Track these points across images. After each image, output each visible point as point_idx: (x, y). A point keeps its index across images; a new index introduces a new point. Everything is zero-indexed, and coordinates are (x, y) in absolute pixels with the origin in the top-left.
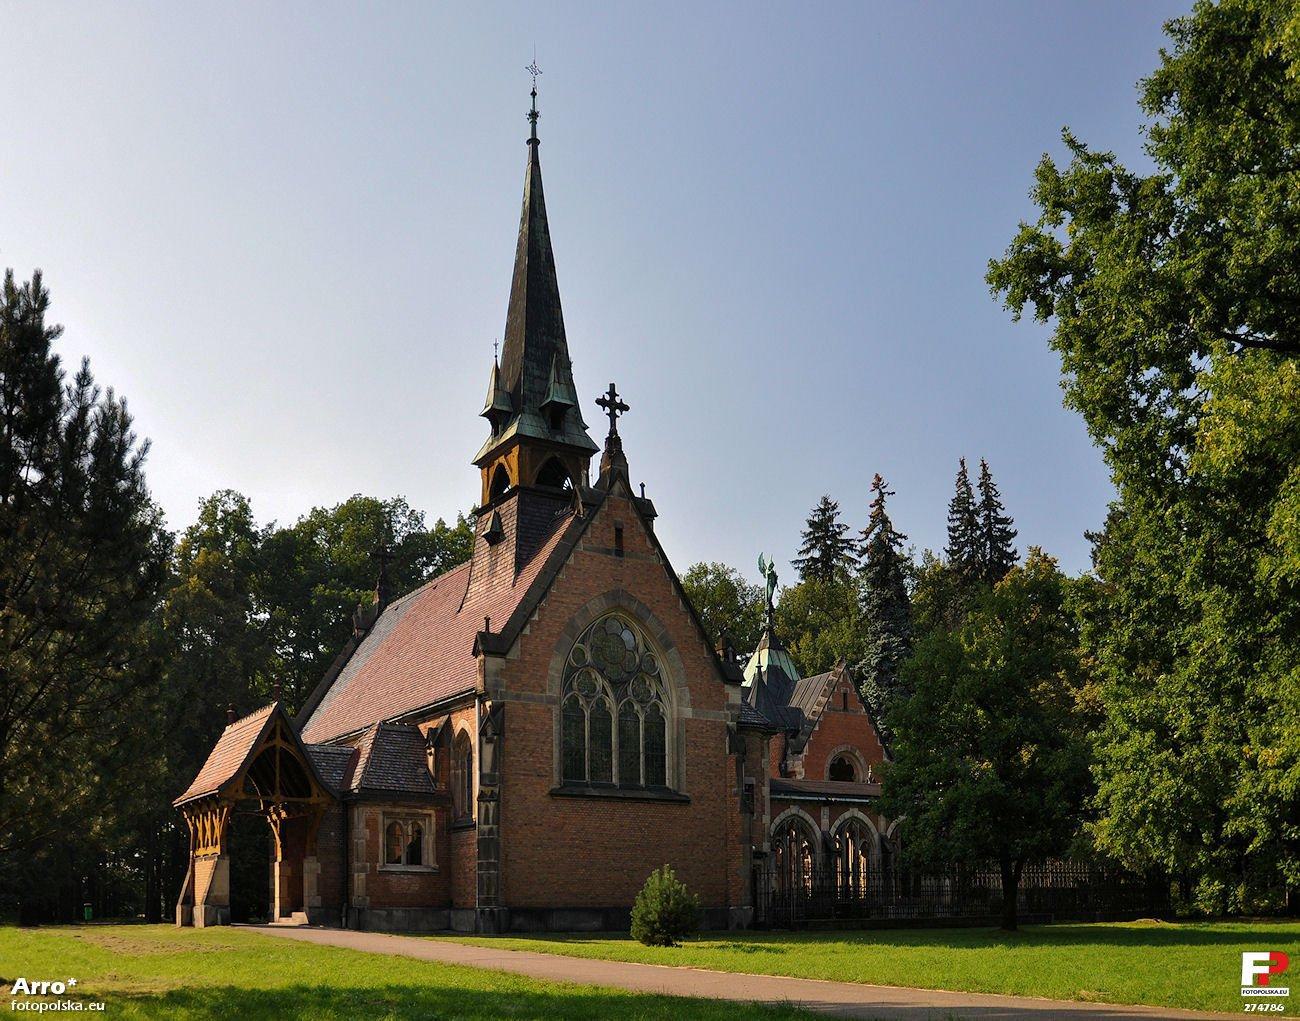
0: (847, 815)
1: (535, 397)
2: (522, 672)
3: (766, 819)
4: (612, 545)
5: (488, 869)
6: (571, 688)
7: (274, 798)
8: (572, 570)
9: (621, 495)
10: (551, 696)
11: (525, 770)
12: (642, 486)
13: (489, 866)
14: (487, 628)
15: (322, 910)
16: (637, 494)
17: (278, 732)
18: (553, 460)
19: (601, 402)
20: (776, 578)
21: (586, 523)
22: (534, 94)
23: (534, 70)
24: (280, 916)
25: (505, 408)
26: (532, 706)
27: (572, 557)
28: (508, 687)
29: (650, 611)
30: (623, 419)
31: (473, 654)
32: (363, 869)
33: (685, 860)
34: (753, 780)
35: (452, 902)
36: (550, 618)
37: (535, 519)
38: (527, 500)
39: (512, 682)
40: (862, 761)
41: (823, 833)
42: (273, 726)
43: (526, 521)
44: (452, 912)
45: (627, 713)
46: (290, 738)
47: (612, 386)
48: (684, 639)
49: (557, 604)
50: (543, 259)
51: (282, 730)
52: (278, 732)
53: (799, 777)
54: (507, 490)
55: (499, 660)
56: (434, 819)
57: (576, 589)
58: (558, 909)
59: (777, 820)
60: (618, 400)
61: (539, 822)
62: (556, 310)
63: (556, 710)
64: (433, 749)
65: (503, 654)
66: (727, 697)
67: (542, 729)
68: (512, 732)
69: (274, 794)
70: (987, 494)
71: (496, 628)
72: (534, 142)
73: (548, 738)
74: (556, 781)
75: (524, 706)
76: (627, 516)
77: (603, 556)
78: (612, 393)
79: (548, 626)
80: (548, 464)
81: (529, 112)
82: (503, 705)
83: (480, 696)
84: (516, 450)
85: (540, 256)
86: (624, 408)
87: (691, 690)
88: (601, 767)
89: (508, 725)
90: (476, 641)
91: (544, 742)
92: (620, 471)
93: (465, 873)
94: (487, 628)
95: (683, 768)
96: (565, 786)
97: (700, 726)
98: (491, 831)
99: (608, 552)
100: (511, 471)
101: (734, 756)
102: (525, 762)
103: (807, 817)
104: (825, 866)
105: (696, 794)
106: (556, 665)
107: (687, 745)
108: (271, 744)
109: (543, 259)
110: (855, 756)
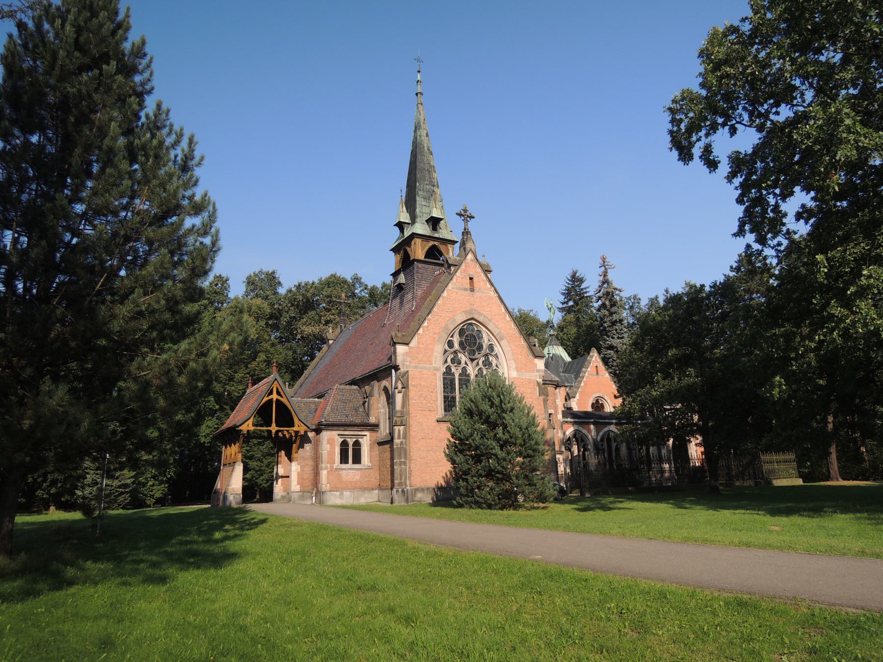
4: (468, 286)
6: (446, 361)
15: (300, 493)
18: (434, 246)
27: (445, 292)
29: (490, 321)
39: (413, 359)
50: (426, 149)
56: (368, 437)
59: (601, 434)
66: (536, 365)
77: (463, 292)
85: (424, 147)
86: (472, 217)
87: (516, 362)
98: (402, 443)
99: (465, 289)
101: (542, 398)
108: (270, 397)
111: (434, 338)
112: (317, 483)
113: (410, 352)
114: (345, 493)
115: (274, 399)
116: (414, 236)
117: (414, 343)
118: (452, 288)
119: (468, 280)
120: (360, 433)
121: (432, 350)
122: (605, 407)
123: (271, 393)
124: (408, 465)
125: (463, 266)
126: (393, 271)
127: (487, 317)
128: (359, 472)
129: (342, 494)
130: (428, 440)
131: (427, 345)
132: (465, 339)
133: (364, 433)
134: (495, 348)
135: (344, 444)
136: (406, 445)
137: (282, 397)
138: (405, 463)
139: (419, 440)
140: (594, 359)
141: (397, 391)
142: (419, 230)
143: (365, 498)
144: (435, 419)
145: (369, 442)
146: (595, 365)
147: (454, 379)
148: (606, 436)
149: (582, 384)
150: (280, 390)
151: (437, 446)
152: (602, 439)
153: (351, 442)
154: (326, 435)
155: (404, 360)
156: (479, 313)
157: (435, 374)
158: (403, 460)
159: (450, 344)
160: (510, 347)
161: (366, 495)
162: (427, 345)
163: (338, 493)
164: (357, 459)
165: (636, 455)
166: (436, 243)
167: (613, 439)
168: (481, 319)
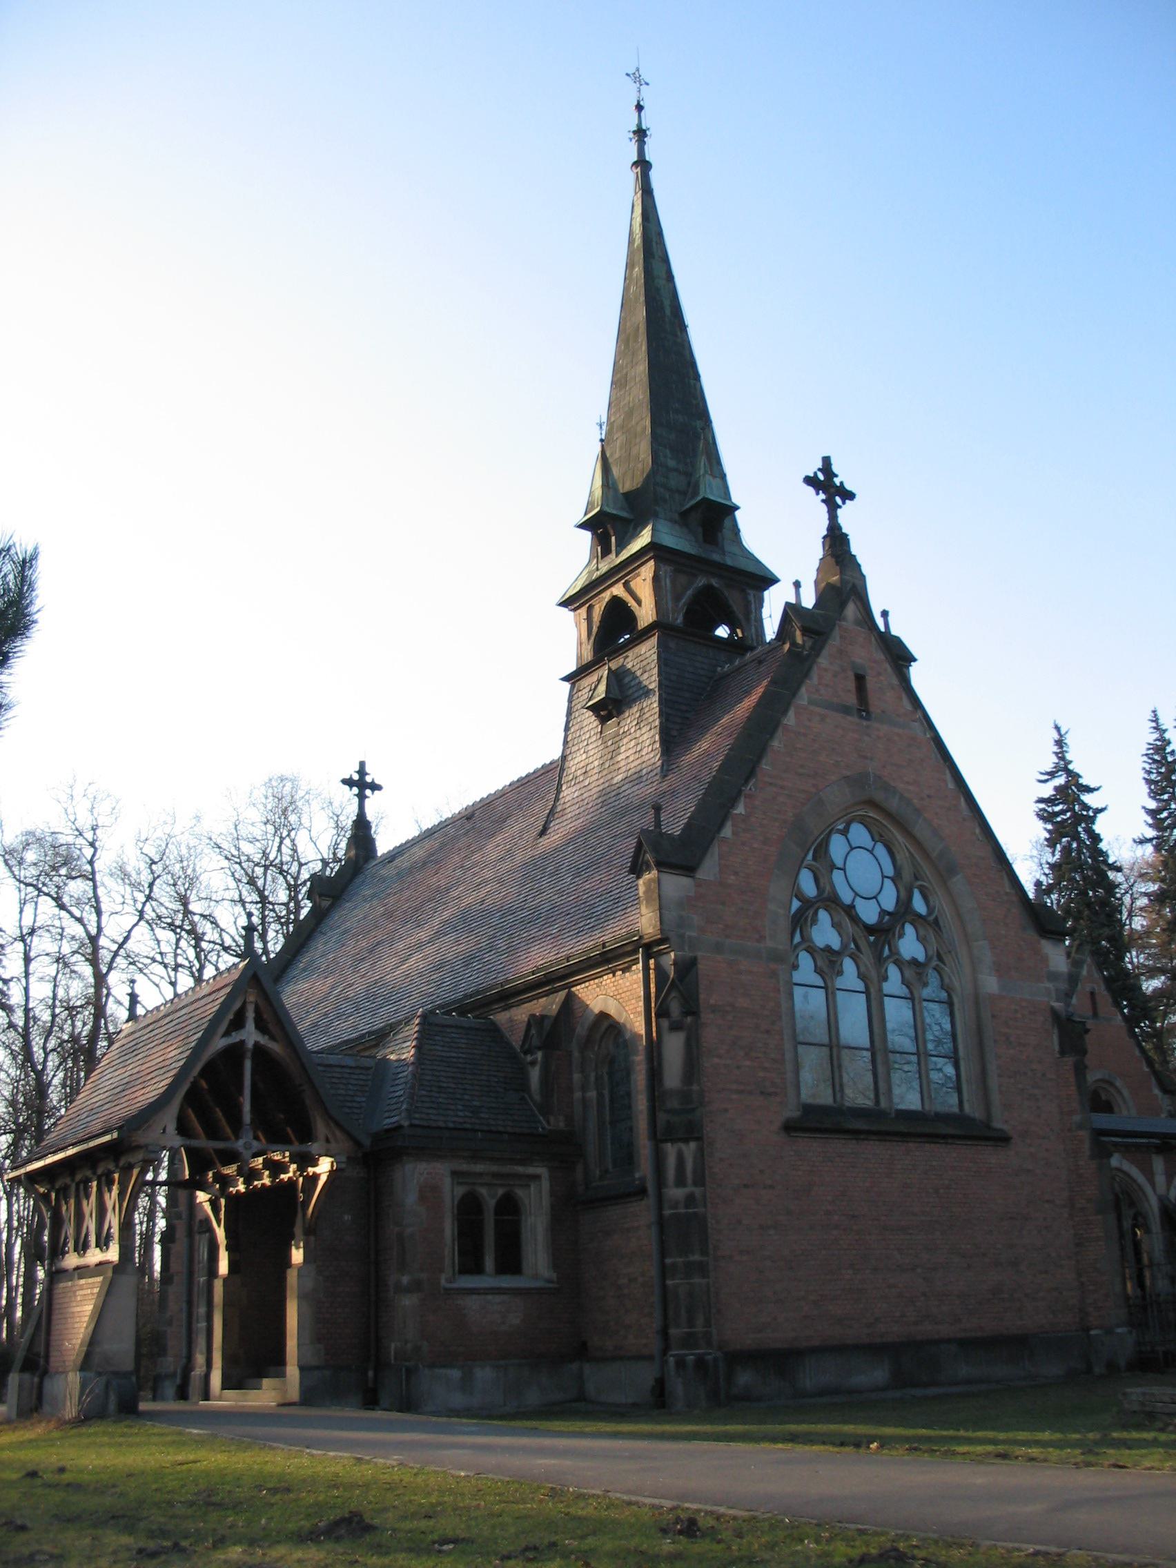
4: (852, 700)
7: (241, 1142)
14: (658, 823)
17: (250, 1015)
18: (709, 588)
23: (637, 77)
24: (224, 1387)
25: (624, 514)
27: (791, 713)
30: (848, 516)
32: (416, 1286)
35: (584, 1344)
38: (672, 645)
40: (1126, 1093)
42: (237, 1005)
47: (362, 764)
51: (257, 1011)
52: (250, 1015)
54: (622, 640)
55: (684, 881)
56: (546, 1184)
57: (802, 766)
58: (814, 1351)
62: (692, 382)
64: (539, 1055)
65: (688, 869)
66: (1045, 959)
68: (713, 1012)
69: (237, 1137)
71: (674, 825)
72: (643, 165)
78: (362, 771)
82: (693, 962)
83: (648, 948)
84: (647, 570)
86: (375, 787)
89: (708, 998)
90: (639, 846)
91: (768, 1032)
94: (658, 823)
95: (994, 1082)
98: (690, 1200)
99: (845, 710)
100: (639, 602)
101: (1070, 1060)
108: (235, 1038)
110: (1116, 1088)
115: (250, 1044)
117: (708, 869)
118: (811, 702)
119: (851, 685)
120: (520, 1169)
123: (238, 1023)
126: (572, 667)
133: (531, 1170)
135: (469, 1209)
137: (273, 1038)
138: (702, 1269)
140: (1084, 972)
145: (546, 1201)
146: (1088, 989)
153: (490, 1198)
158: (696, 1257)
163: (455, 1374)
164: (510, 1262)
166: (714, 582)
168: (893, 804)
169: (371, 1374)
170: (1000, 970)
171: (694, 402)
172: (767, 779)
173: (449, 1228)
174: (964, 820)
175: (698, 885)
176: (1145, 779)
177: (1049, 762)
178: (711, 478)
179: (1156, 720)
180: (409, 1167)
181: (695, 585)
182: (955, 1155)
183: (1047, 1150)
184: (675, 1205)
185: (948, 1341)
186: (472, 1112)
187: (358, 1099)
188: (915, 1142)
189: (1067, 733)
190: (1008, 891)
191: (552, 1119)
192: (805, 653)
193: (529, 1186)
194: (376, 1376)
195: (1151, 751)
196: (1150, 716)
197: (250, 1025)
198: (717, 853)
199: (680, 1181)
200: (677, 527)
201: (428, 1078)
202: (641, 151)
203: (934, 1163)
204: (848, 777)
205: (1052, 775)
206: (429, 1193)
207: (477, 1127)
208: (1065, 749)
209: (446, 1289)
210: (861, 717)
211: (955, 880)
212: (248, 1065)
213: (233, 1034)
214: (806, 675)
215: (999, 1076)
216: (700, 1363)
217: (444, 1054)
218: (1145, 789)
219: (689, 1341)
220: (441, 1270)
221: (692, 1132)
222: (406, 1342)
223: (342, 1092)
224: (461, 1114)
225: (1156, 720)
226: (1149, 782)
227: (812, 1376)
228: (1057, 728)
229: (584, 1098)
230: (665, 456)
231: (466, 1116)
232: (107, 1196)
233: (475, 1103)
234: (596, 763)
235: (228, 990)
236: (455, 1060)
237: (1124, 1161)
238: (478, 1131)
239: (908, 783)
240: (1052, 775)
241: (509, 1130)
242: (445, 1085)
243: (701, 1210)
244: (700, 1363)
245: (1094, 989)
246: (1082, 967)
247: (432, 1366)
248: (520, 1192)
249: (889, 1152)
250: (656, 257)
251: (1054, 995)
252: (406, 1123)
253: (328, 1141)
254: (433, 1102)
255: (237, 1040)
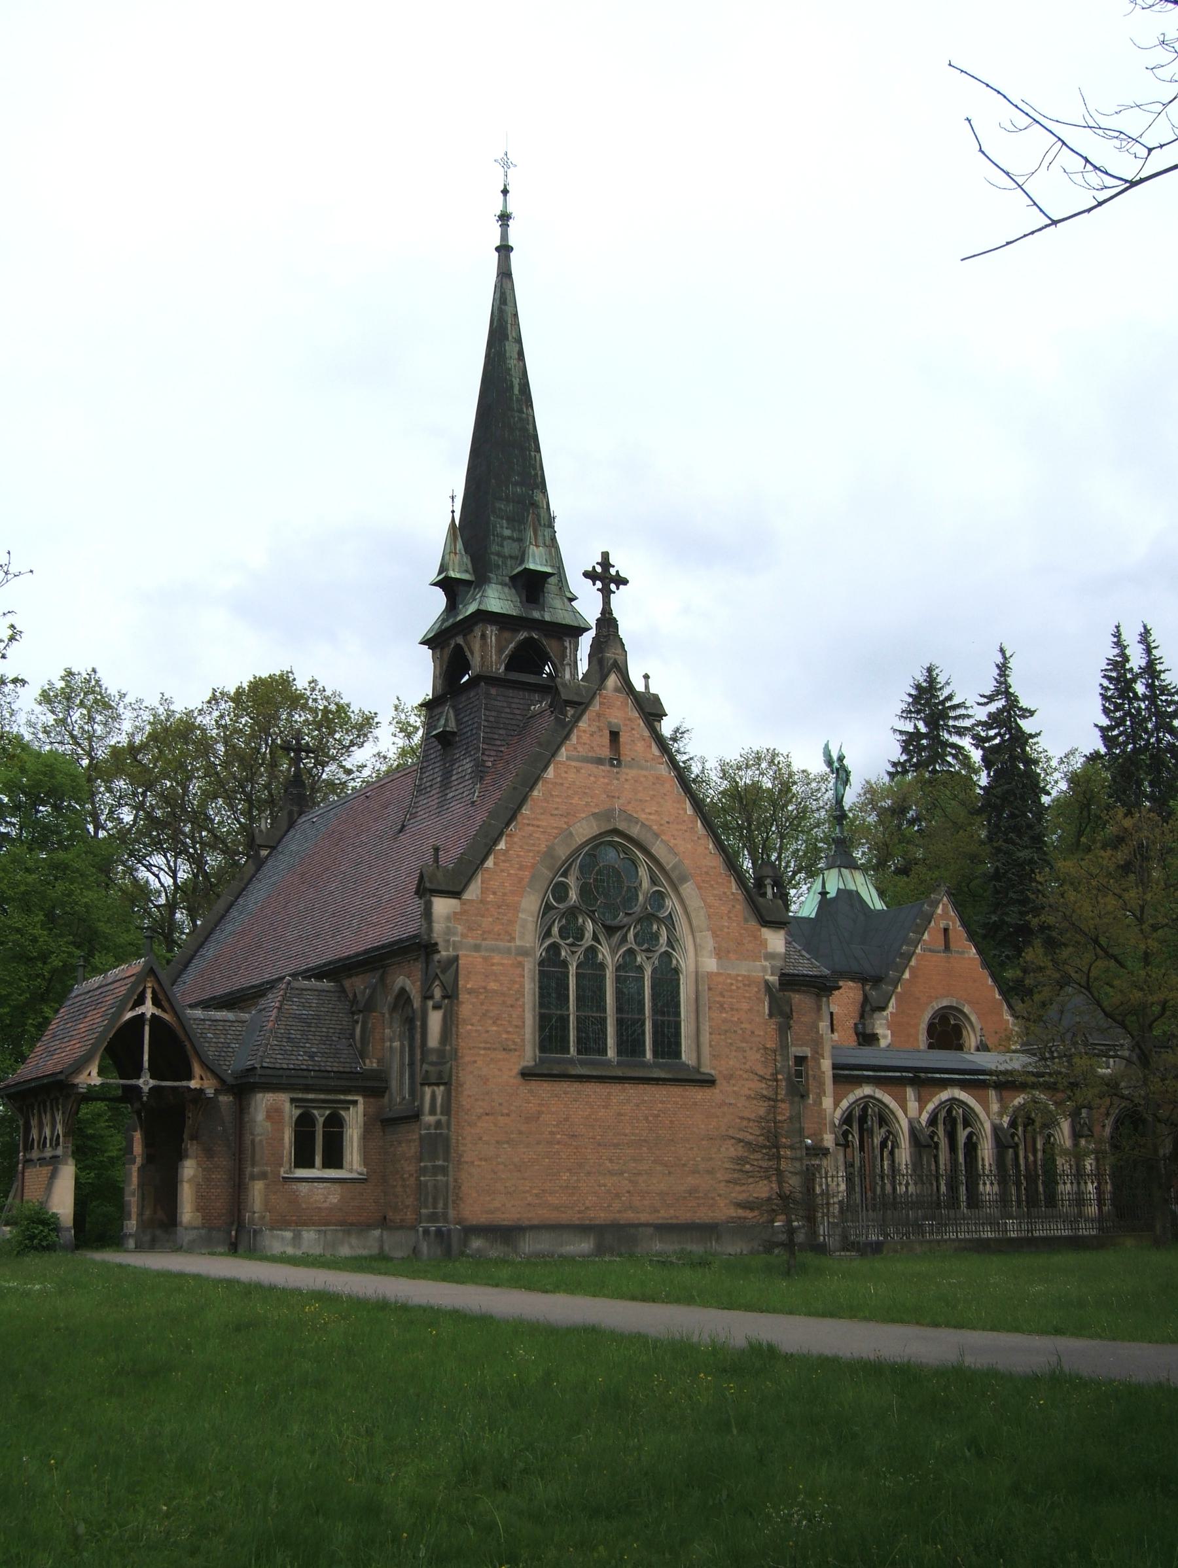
0: (945, 1095)
1: (505, 563)
2: (483, 916)
3: (827, 1102)
4: (606, 752)
5: (435, 1174)
6: (548, 934)
8: (551, 786)
9: (617, 690)
10: (522, 946)
11: (486, 1042)
12: (646, 677)
13: (437, 1170)
16: (639, 686)
17: (149, 995)
18: (529, 641)
19: (590, 575)
20: (848, 773)
21: (570, 726)
22: (505, 192)
26: (497, 959)
27: (551, 769)
28: (463, 936)
29: (657, 836)
31: (417, 893)
33: (711, 1159)
34: (807, 1051)
36: (521, 847)
37: (503, 715)
39: (470, 929)
41: (910, 1122)
43: (492, 719)
44: (385, 1232)
45: (627, 965)
46: (165, 1004)
47: (605, 556)
48: (705, 869)
49: (531, 828)
50: (516, 391)
51: (154, 992)
52: (149, 995)
53: (883, 1043)
55: (453, 902)
56: (361, 1107)
57: (557, 809)
59: (845, 1104)
60: (613, 571)
61: (506, 1111)
63: (530, 966)
66: (764, 943)
67: (510, 989)
68: (469, 993)
70: (1149, 650)
72: (504, 250)
73: (517, 1000)
74: (529, 1055)
75: (485, 959)
76: (623, 714)
77: (592, 767)
78: (605, 562)
79: (518, 856)
80: (522, 645)
81: (498, 213)
85: (512, 387)
86: (621, 581)
87: (715, 935)
88: (592, 1042)
91: (512, 1006)
92: (615, 661)
93: (404, 1180)
95: (705, 1038)
96: (542, 1061)
97: (729, 981)
98: (438, 1124)
99: (599, 761)
102: (487, 1032)
103: (887, 1099)
104: (914, 1165)
105: (725, 1072)
106: (530, 904)
107: (710, 1008)
108: (139, 1011)
109: (516, 391)
111: (521, 880)
112: (239, 1211)
113: (463, 912)
114: (305, 1234)
115: (148, 1015)
116: (483, 616)
117: (473, 892)
118: (568, 758)
119: (606, 740)
120: (342, 1097)
121: (516, 908)
122: (965, 1033)
123: (140, 1001)
124: (451, 1173)
125: (595, 707)
127: (649, 828)
128: (337, 1186)
129: (297, 1237)
130: (500, 1118)
131: (504, 894)
132: (596, 880)
133: (355, 1098)
134: (668, 903)
135: (304, 1126)
136: (449, 1128)
137: (164, 1010)
138: (444, 1170)
139: (479, 1117)
140: (939, 911)
141: (430, 1003)
142: (493, 601)
143: (352, 1247)
144: (516, 1069)
145: (361, 1119)
147: (566, 975)
148: (943, 1114)
149: (907, 975)
150: (161, 996)
151: (520, 1133)
152: (933, 1121)
153: (320, 1116)
154: (263, 1102)
155: (449, 931)
156: (631, 819)
157: (521, 965)
158: (440, 1163)
159: (560, 891)
160: (704, 901)
161: (354, 1241)
162: (504, 894)
163: (288, 1235)
164: (334, 1158)
165: (1017, 1165)
167: (960, 1121)
168: (634, 831)
169: (233, 1233)
170: (719, 953)
171: (533, 472)
172: (525, 821)
173: (288, 1136)
174: (699, 838)
175: (463, 904)
176: (1101, 694)
177: (989, 688)
178: (535, 548)
179: (1118, 635)
180: (259, 1096)
181: (518, 639)
182: (665, 1093)
183: (749, 1089)
184: (428, 1127)
185: (647, 1225)
186: (309, 1057)
187: (233, 1045)
188: (629, 1083)
189: (1011, 656)
190: (734, 891)
191: (367, 1061)
192: (567, 719)
193: (349, 1108)
194: (236, 1234)
195: (1109, 667)
196: (1113, 630)
197: (149, 1002)
198: (480, 881)
199: (433, 1112)
200: (506, 590)
201: (282, 1031)
202: (504, 236)
203: (646, 1098)
204: (595, 813)
205: (991, 699)
206: (274, 1114)
207: (311, 1068)
208: (1007, 673)
209: (283, 1178)
210: (612, 765)
211: (685, 886)
212: (147, 1028)
213: (137, 1009)
214: (567, 737)
215: (710, 1034)
216: (439, 1232)
217: (297, 1012)
218: (1098, 703)
219: (433, 1218)
220: (281, 1165)
221: (444, 1081)
222: (254, 1213)
223: (223, 1040)
224: (301, 1058)
225: (1118, 635)
226: (1105, 698)
227: (529, 1245)
228: (1002, 651)
229: (391, 1047)
230: (502, 527)
231: (304, 1060)
232: (56, 1114)
233: (313, 1050)
234: (439, 779)
235: (132, 979)
236: (305, 1017)
237: (877, 1090)
238: (311, 1071)
239: (650, 814)
240: (991, 699)
241: (335, 1069)
242: (293, 1036)
243: (445, 1131)
244: (439, 1232)
245: (948, 925)
246: (937, 907)
247: (272, 1229)
248: (342, 1113)
249: (608, 1090)
250: (510, 338)
251: (769, 971)
252: (258, 1066)
253: (202, 1079)
254: (282, 1050)
255: (140, 1013)
